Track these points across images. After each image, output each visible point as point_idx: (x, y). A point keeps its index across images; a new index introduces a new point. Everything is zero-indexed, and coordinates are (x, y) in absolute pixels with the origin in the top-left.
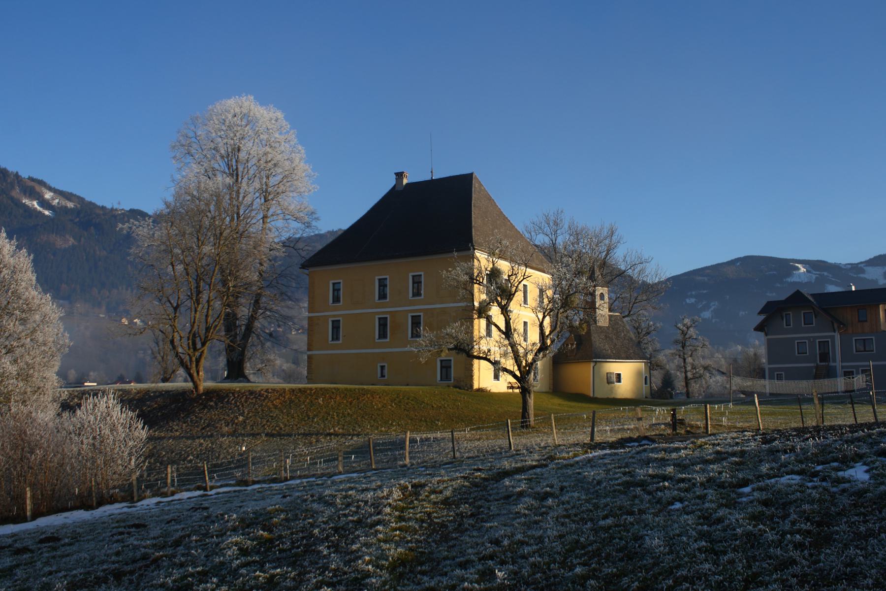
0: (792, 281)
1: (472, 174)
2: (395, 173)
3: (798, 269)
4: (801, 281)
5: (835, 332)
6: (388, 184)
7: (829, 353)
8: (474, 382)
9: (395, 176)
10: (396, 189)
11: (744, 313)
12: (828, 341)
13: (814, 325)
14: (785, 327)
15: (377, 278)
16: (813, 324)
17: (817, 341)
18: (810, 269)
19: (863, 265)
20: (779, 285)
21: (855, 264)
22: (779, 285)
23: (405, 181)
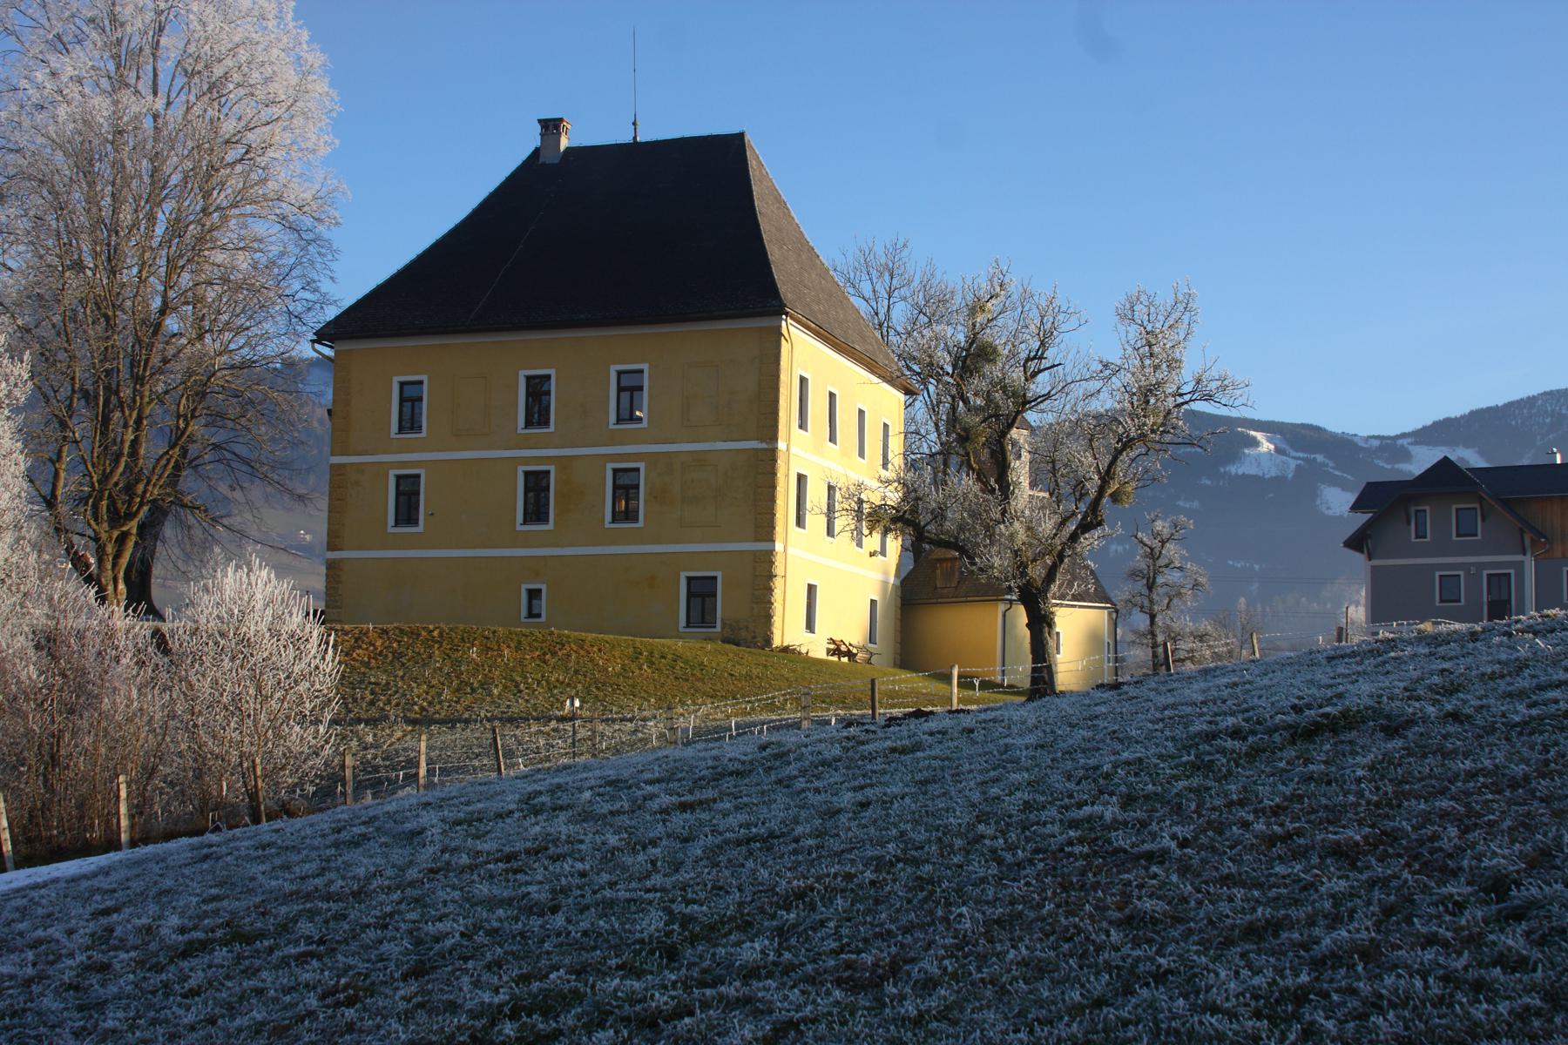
0: (1240, 473)
1: (741, 136)
2: (540, 121)
3: (1254, 443)
4: (1261, 474)
5: (1524, 554)
6: (523, 143)
7: (1509, 601)
8: (775, 631)
9: (538, 128)
10: (541, 160)
11: (1120, 548)
12: (1509, 574)
13: (1479, 537)
14: (1413, 540)
15: (523, 374)
16: (1476, 535)
17: (1485, 573)
18: (1284, 446)
19: (1409, 440)
20: (1208, 482)
21: (1388, 438)
22: (1208, 482)
23: (564, 143)
